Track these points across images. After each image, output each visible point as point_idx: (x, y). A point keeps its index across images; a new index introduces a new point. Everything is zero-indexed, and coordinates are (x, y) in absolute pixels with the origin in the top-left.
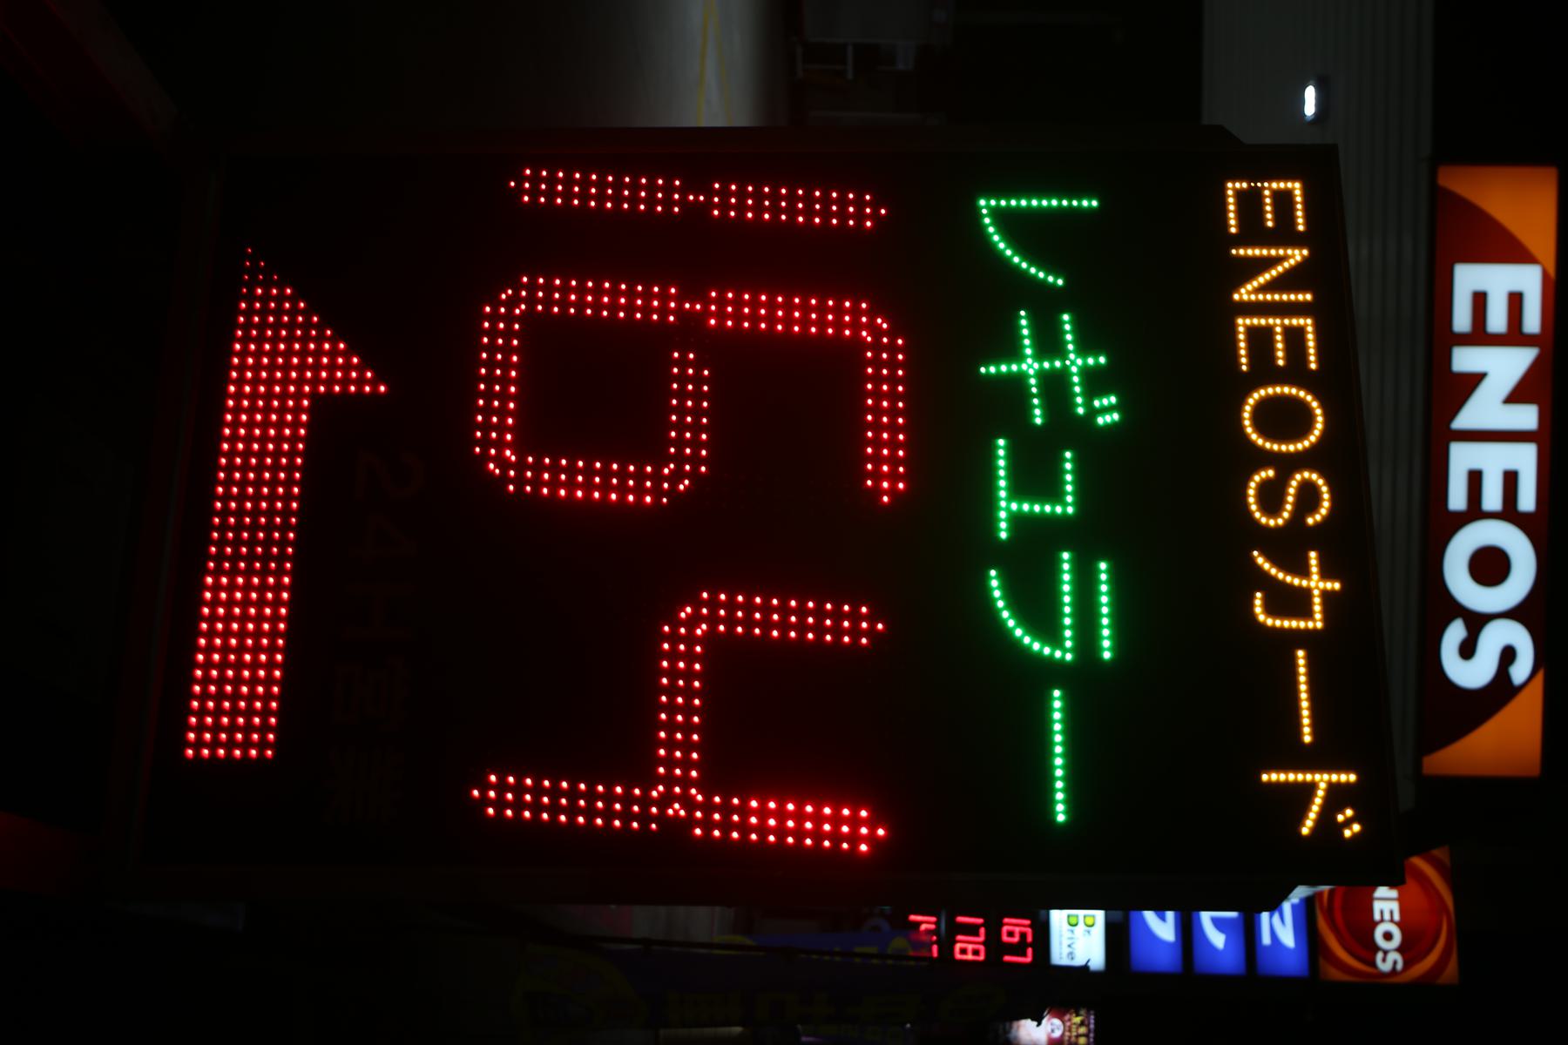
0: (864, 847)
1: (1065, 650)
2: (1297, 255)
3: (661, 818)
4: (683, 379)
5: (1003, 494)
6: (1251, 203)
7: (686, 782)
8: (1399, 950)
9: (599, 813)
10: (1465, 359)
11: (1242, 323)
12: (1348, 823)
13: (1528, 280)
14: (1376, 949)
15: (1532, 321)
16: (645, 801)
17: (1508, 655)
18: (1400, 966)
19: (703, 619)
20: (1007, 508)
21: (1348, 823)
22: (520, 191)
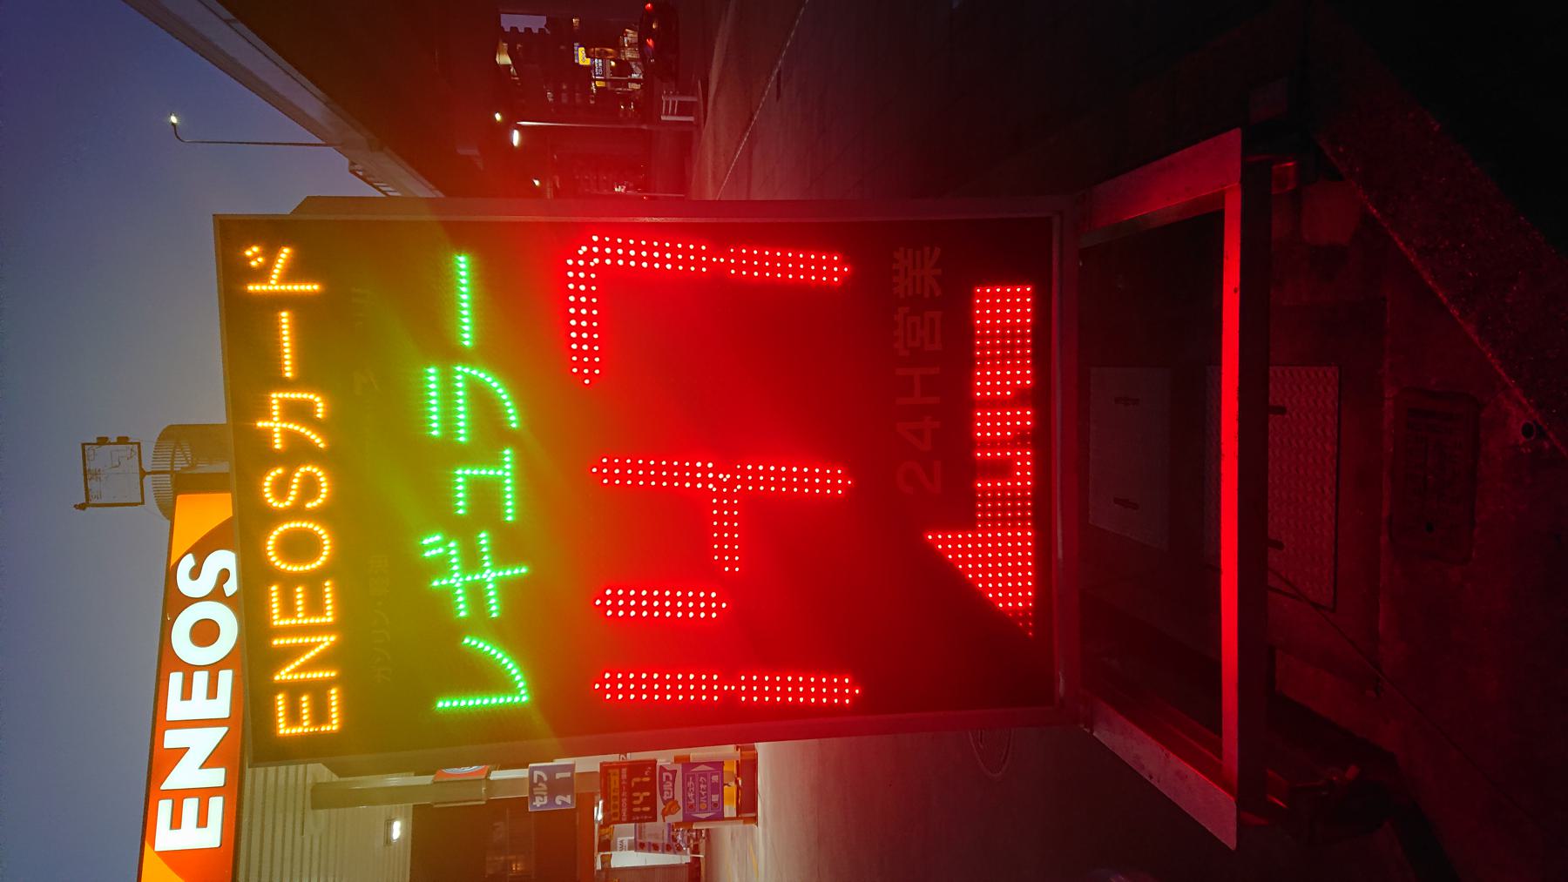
0: (595, 238)
2: (284, 675)
3: (734, 472)
4: (731, 552)
5: (508, 481)
6: (320, 715)
7: (720, 495)
10: (216, 777)
11: (329, 618)
12: (255, 256)
13: (166, 839)
15: (165, 808)
16: (744, 482)
17: (195, 573)
19: (720, 490)
21: (255, 256)
22: (851, 686)
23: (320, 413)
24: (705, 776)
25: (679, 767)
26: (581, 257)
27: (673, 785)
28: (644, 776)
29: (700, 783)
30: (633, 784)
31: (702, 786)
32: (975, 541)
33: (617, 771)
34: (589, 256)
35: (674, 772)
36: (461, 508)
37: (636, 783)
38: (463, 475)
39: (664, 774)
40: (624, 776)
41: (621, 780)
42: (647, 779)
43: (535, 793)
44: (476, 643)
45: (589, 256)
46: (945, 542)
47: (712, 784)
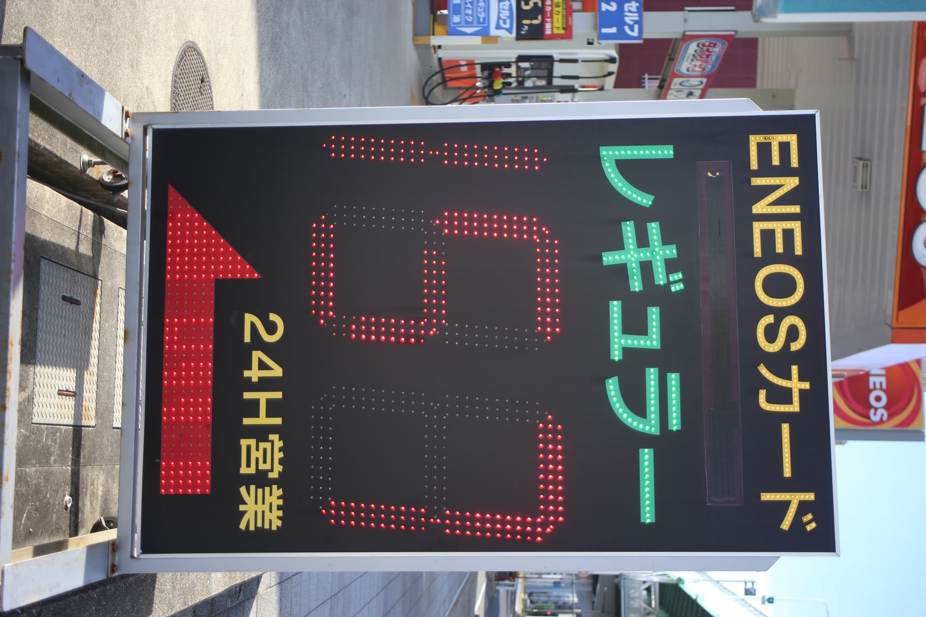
6: (765, 149)
8: (886, 407)
9: (392, 522)
11: (758, 227)
14: (870, 407)
18: (885, 418)
23: (762, 394)
24: (467, 22)
25: (493, 32)
26: (552, 523)
27: (499, 13)
28: (530, 26)
29: (472, 16)
30: (540, 17)
31: (470, 12)
32: (217, 271)
33: (556, 31)
34: (545, 524)
35: (498, 27)
36: (654, 315)
37: (536, 19)
38: (652, 341)
39: (508, 26)
40: (548, 26)
41: (552, 22)
42: (526, 22)
43: (636, 15)
44: (644, 200)
45: (545, 524)
46: (243, 271)
47: (460, 14)
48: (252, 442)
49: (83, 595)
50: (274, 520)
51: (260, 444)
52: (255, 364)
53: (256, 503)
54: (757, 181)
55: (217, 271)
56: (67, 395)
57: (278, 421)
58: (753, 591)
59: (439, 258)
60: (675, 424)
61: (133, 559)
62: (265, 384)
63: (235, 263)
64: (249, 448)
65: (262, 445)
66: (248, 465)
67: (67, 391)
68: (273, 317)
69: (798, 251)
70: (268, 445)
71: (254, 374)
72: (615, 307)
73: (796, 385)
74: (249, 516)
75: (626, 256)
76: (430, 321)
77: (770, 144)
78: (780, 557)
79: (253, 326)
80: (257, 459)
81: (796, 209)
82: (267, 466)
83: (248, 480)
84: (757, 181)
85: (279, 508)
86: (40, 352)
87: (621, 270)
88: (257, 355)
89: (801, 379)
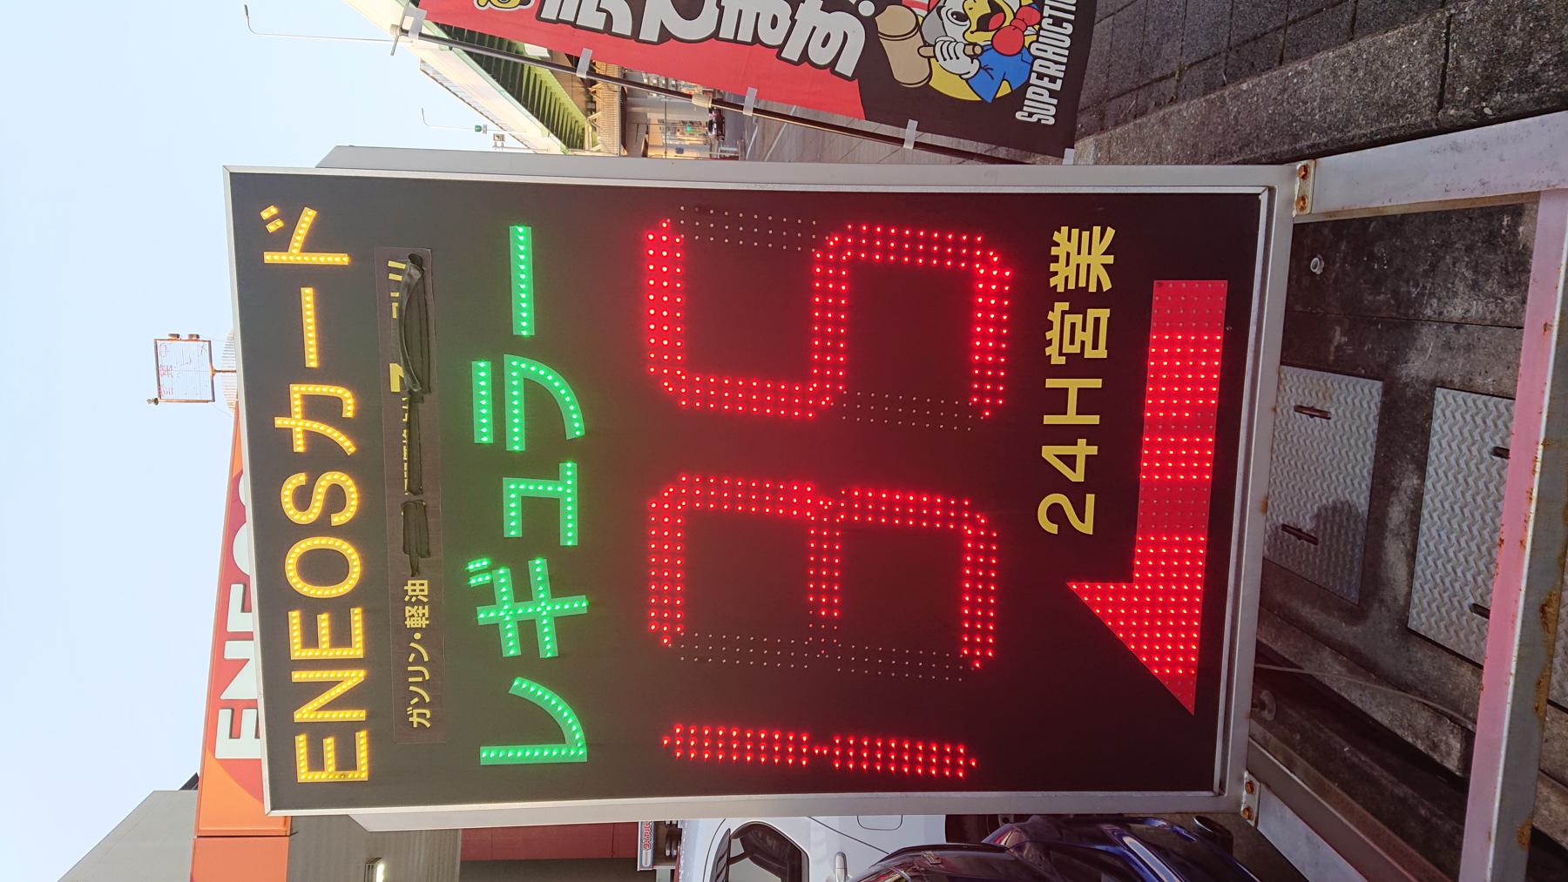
1: (518, 369)
6: (346, 760)
11: (357, 650)
16: (857, 247)
20: (565, 487)
22: (966, 757)
32: (1130, 593)
36: (513, 527)
38: (516, 490)
44: (523, 686)
46: (1092, 593)
48: (1089, 353)
49: (1339, 136)
50: (1064, 241)
51: (1079, 352)
52: (1081, 464)
53: (1089, 266)
54: (359, 715)
55: (1130, 593)
56: (1312, 409)
57: (1051, 383)
58: (496, 138)
59: (817, 604)
60: (482, 371)
61: (1271, 185)
62: (1067, 435)
63: (1104, 605)
64: (1095, 347)
65: (1076, 349)
66: (1097, 320)
67: (1312, 416)
68: (1052, 528)
69: (295, 617)
70: (1067, 349)
71: (1083, 450)
72: (569, 536)
73: (297, 425)
74: (1100, 247)
75: (543, 617)
76: (832, 520)
77: (338, 769)
78: (317, 167)
79: (1082, 520)
80: (1084, 329)
81: (297, 676)
82: (1069, 319)
83: (1099, 299)
84: (359, 715)
85: (1056, 259)
86: (1363, 477)
87: (559, 588)
88: (1078, 476)
89: (288, 433)
